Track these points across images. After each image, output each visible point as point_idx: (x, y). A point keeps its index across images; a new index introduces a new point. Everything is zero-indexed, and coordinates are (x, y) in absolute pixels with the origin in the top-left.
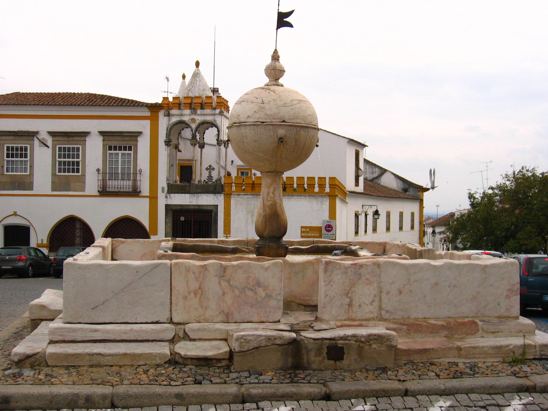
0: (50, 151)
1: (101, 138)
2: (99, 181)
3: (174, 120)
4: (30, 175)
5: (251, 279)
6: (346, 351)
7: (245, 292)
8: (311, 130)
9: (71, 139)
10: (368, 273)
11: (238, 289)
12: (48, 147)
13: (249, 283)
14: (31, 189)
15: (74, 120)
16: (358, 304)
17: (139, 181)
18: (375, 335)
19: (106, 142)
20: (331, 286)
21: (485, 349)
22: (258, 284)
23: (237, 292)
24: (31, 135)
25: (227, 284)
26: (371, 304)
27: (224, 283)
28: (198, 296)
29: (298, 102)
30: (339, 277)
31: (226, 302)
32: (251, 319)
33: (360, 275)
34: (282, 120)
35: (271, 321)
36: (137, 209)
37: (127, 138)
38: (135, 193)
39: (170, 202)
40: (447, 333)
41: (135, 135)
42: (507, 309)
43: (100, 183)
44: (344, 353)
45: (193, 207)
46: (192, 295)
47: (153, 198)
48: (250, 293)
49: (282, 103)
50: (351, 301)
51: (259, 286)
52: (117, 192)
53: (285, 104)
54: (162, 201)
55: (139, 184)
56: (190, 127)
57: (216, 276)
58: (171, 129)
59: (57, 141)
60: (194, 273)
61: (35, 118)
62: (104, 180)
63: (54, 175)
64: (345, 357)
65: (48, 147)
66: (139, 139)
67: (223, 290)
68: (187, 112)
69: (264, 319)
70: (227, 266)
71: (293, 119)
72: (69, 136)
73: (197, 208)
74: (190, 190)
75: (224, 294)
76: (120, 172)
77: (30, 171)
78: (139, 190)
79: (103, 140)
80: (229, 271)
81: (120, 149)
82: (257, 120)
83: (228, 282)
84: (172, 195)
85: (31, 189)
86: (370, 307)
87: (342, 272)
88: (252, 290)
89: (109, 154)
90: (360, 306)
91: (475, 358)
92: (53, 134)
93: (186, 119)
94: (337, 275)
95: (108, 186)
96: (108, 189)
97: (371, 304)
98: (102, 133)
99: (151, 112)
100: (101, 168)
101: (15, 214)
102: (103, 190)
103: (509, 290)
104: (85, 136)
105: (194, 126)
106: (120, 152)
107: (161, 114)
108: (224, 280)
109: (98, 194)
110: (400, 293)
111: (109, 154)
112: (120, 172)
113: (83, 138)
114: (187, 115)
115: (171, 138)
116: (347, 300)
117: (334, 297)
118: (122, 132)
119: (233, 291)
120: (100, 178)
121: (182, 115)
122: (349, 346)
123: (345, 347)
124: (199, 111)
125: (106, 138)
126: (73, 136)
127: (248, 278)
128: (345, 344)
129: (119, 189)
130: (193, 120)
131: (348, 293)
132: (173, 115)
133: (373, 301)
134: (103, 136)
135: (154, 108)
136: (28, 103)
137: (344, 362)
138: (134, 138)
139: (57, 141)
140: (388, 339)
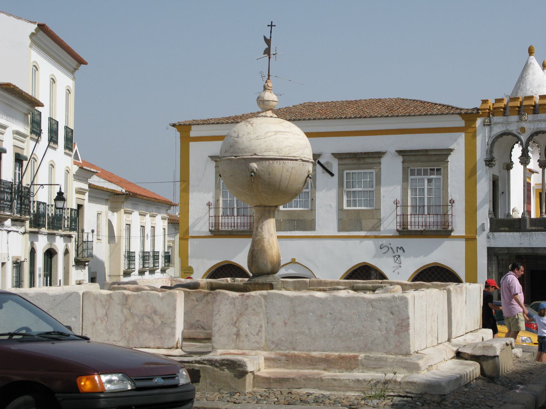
0: (336, 178)
1: (400, 159)
2: (398, 217)
3: (497, 130)
4: (311, 210)
5: (149, 307)
6: (202, 374)
7: (143, 320)
8: (287, 161)
9: (362, 161)
10: (255, 304)
11: (138, 316)
12: (332, 175)
13: (147, 312)
14: (313, 228)
15: (406, 135)
16: (244, 334)
17: (450, 216)
18: (227, 360)
19: (406, 165)
20: (220, 315)
21: (347, 382)
22: (155, 312)
23: (137, 320)
24: (373, 158)
25: (128, 311)
26: (257, 334)
27: (126, 311)
28: (104, 323)
29: (274, 133)
30: (227, 307)
31: (127, 328)
32: (148, 345)
33: (247, 305)
34: (253, 154)
35: (166, 347)
36: (448, 253)
37: (434, 158)
38: (444, 232)
39: (495, 244)
40: (326, 366)
41: (442, 156)
42: (396, 346)
43: (213, 220)
44: (200, 376)
45: (524, 251)
46: (99, 321)
47: (470, 239)
48: (147, 321)
49: (255, 136)
50: (238, 331)
51: (156, 314)
52: (421, 231)
53: (257, 137)
54: (483, 243)
55: (450, 220)
56: (520, 139)
57: (119, 304)
58: (493, 143)
59: (344, 164)
60: (101, 301)
61: (323, 136)
62: (404, 215)
63: (340, 209)
64: (201, 379)
65: (332, 175)
66: (450, 158)
67: (125, 317)
68: (515, 118)
69: (160, 346)
70: (129, 295)
71: (265, 151)
72: (359, 159)
73: (530, 251)
74: (520, 228)
75: (126, 321)
76: (426, 204)
77: (312, 205)
78: (450, 228)
79: (403, 162)
80: (130, 301)
81: (426, 173)
82: (231, 155)
83: (130, 309)
84: (496, 234)
85: (313, 228)
86: (256, 337)
87: (230, 303)
88: (149, 318)
89: (411, 179)
90: (246, 335)
91: (334, 390)
92: (339, 156)
93: (513, 128)
94: (226, 305)
95: (409, 223)
96: (409, 227)
97: (257, 334)
98: (401, 152)
99: (465, 121)
100: (399, 199)
101: (293, 262)
102: (403, 228)
103: (398, 325)
104: (380, 157)
105: (524, 138)
106: (426, 178)
107: (479, 122)
108: (126, 308)
109: (209, 234)
110: (286, 324)
111: (411, 179)
112: (426, 204)
113: (377, 160)
114: (512, 123)
115: (495, 155)
116: (235, 330)
117: (223, 326)
118: (427, 151)
119: (133, 318)
120: (212, 213)
121: (508, 123)
122: (205, 369)
123: (201, 370)
124: (530, 117)
125: (345, 162)
126: (364, 158)
127: (146, 306)
128: (201, 367)
129: (233, 228)
130: (523, 130)
131: (236, 322)
132: (496, 124)
133: (259, 331)
134: (402, 156)
135: (470, 116)
136: (379, 116)
137: (200, 383)
138: (443, 157)
139: (344, 164)
140: (239, 364)
